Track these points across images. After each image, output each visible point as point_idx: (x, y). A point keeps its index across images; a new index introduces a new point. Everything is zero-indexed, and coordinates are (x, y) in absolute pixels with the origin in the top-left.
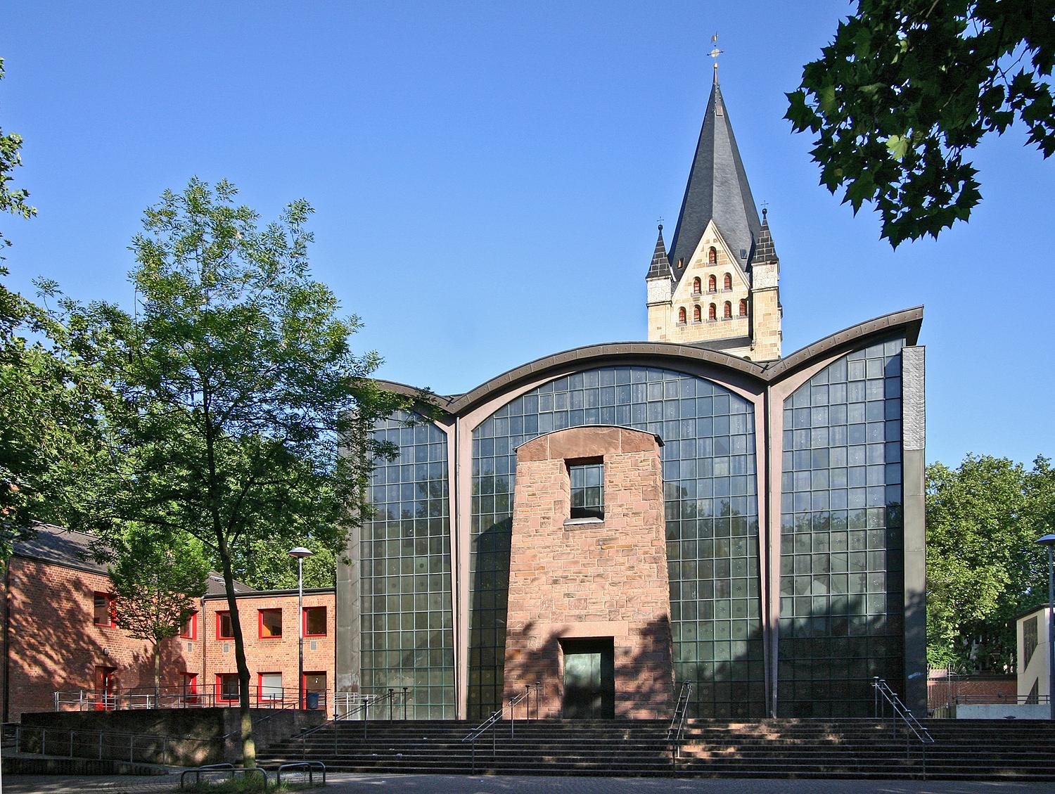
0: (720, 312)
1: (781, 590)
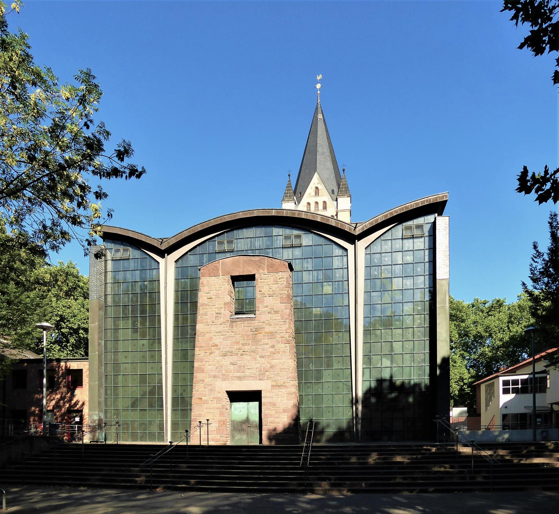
1: (363, 364)
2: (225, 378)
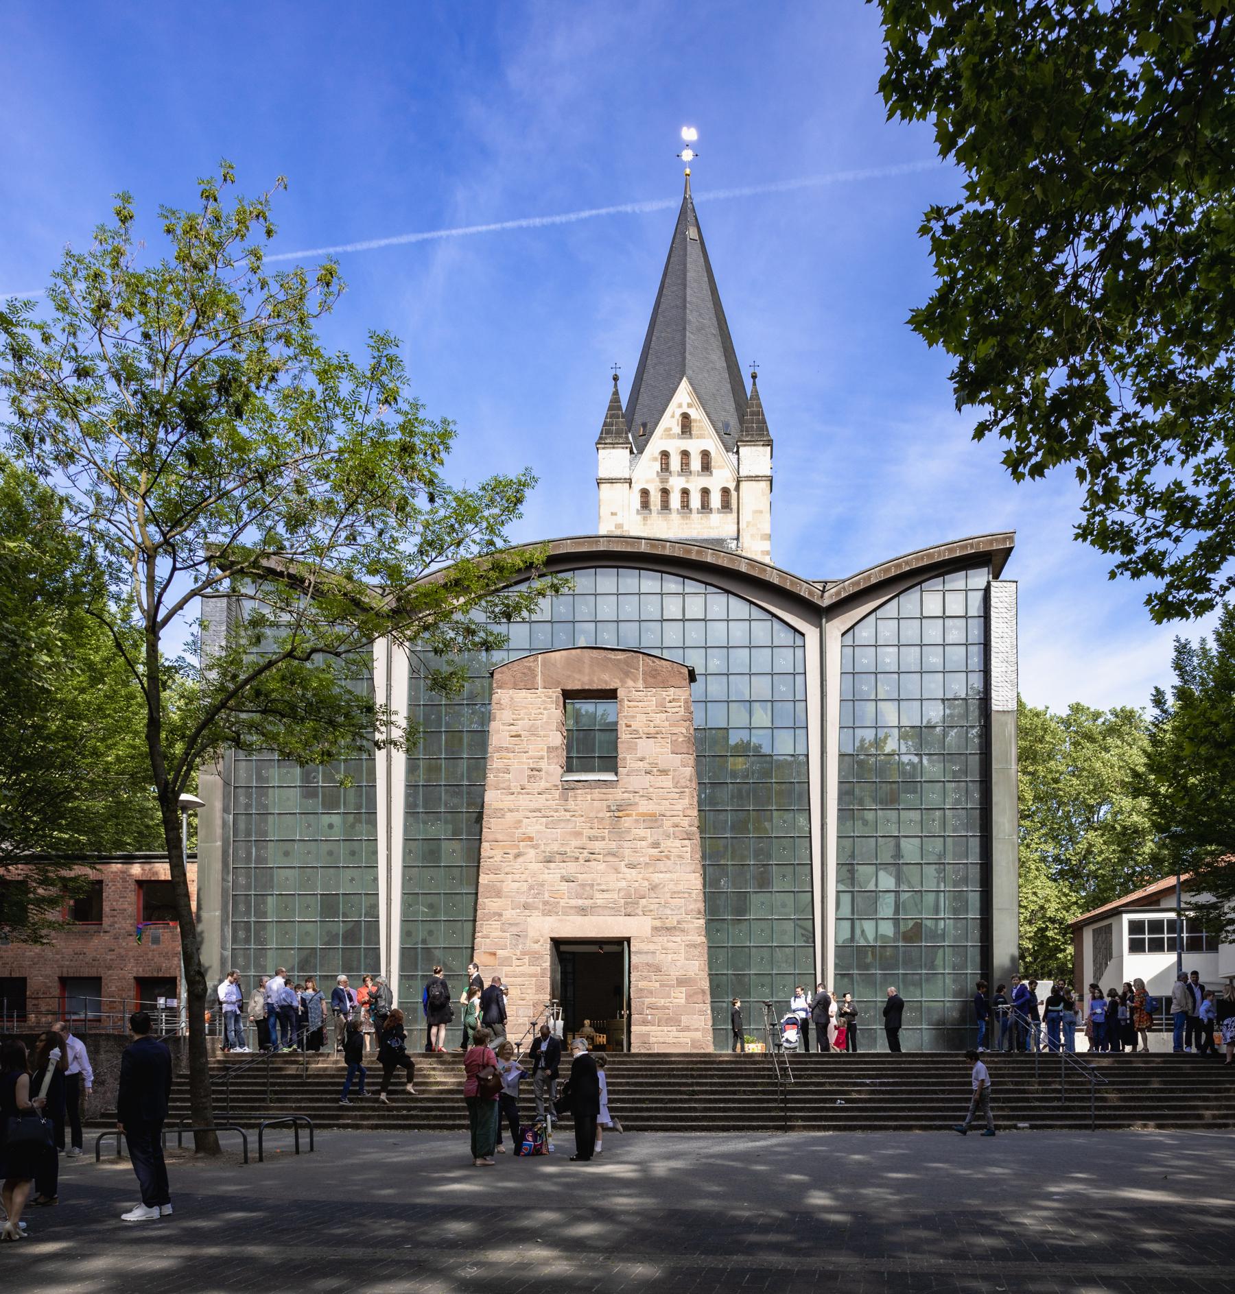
0: (695, 501)
1: (837, 882)
2: (550, 909)
